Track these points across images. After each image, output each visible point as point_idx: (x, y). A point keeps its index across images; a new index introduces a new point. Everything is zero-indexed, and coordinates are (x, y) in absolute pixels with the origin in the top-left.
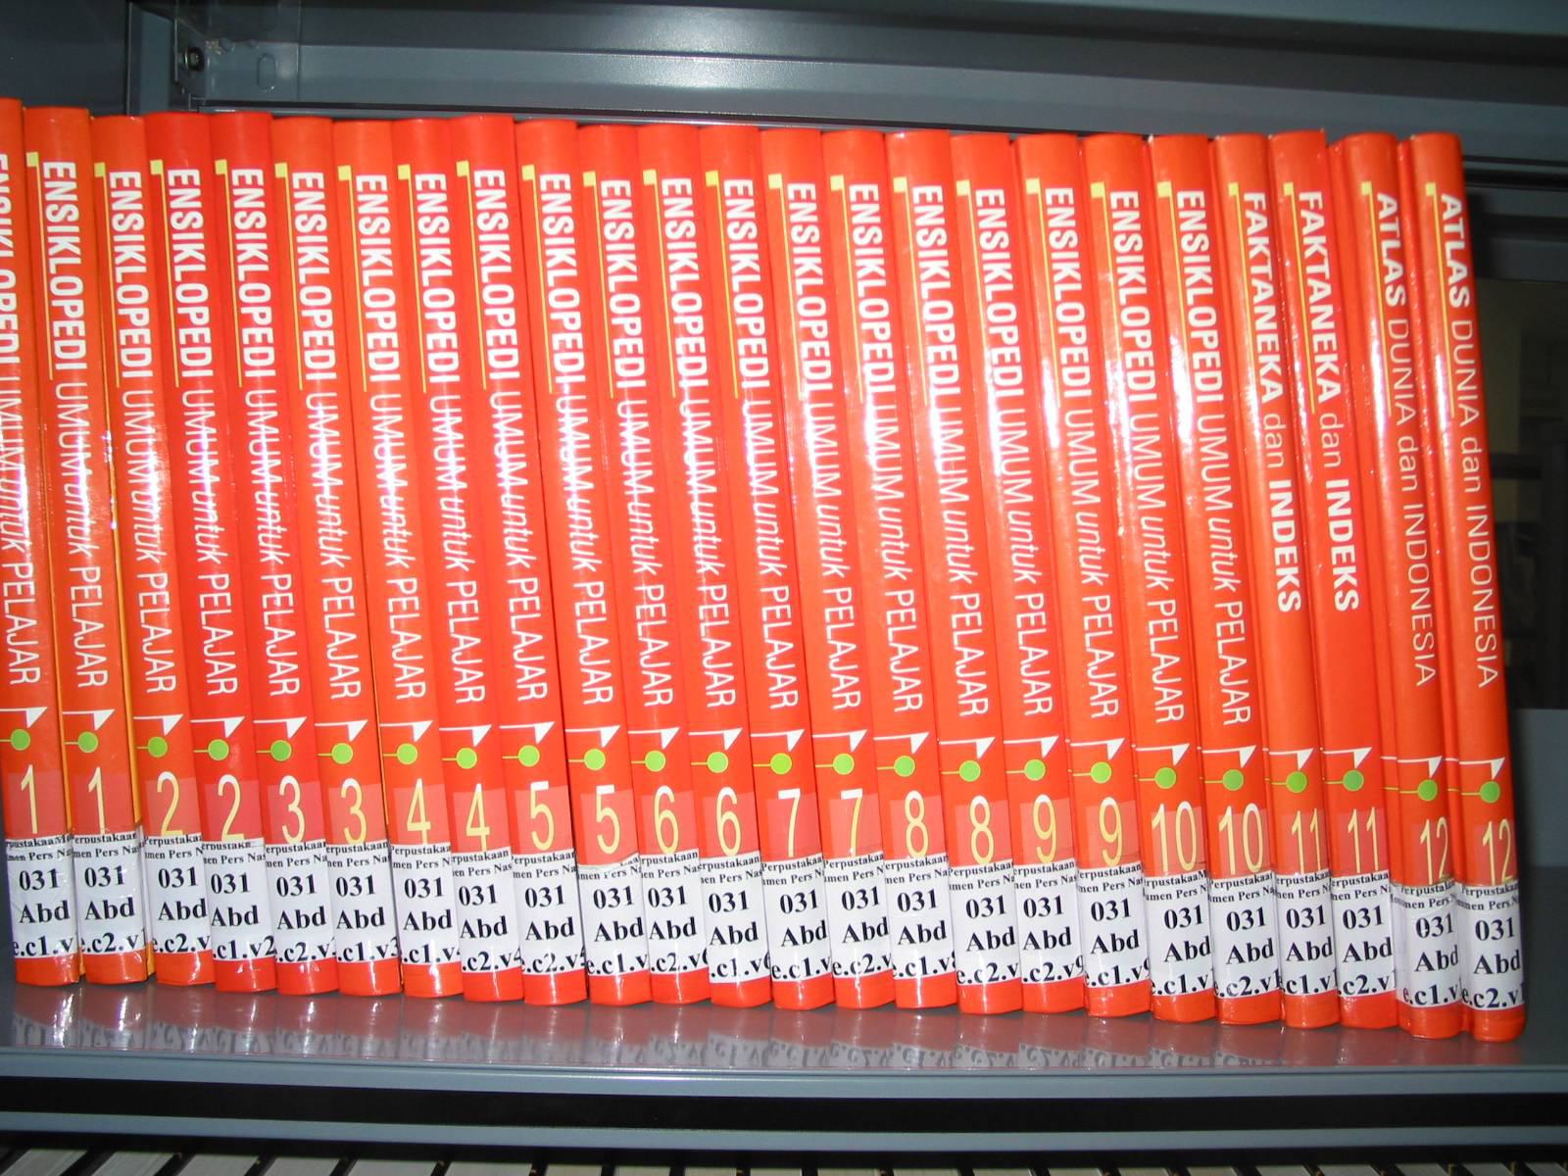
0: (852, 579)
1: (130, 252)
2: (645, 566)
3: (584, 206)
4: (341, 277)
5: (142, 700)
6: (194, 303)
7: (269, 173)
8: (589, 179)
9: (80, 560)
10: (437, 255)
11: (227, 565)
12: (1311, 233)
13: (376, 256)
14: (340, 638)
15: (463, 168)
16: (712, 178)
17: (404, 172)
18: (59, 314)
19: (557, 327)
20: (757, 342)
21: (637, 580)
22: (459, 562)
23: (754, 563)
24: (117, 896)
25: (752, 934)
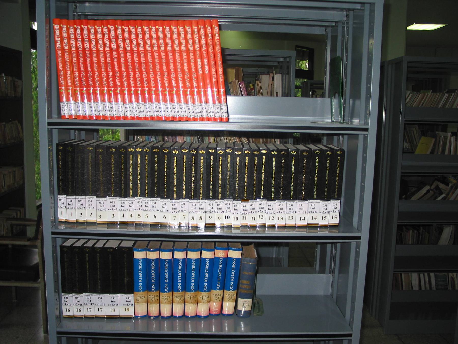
0: (146, 71)
1: (72, 36)
2: (124, 70)
3: (178, 30)
4: (172, 39)
5: (110, 87)
6: (155, 42)
7: (95, 27)
8: (103, 26)
9: (68, 70)
10: (134, 36)
11: (188, 72)
12: (202, 32)
13: (100, 36)
14: (90, 78)
15: (96, 26)
16: (186, 27)
17: (75, 26)
18: (72, 44)
19: (190, 44)
20: (149, 45)
21: (118, 71)
22: (110, 70)
23: (149, 70)
24: (142, 110)
25: (143, 111)
